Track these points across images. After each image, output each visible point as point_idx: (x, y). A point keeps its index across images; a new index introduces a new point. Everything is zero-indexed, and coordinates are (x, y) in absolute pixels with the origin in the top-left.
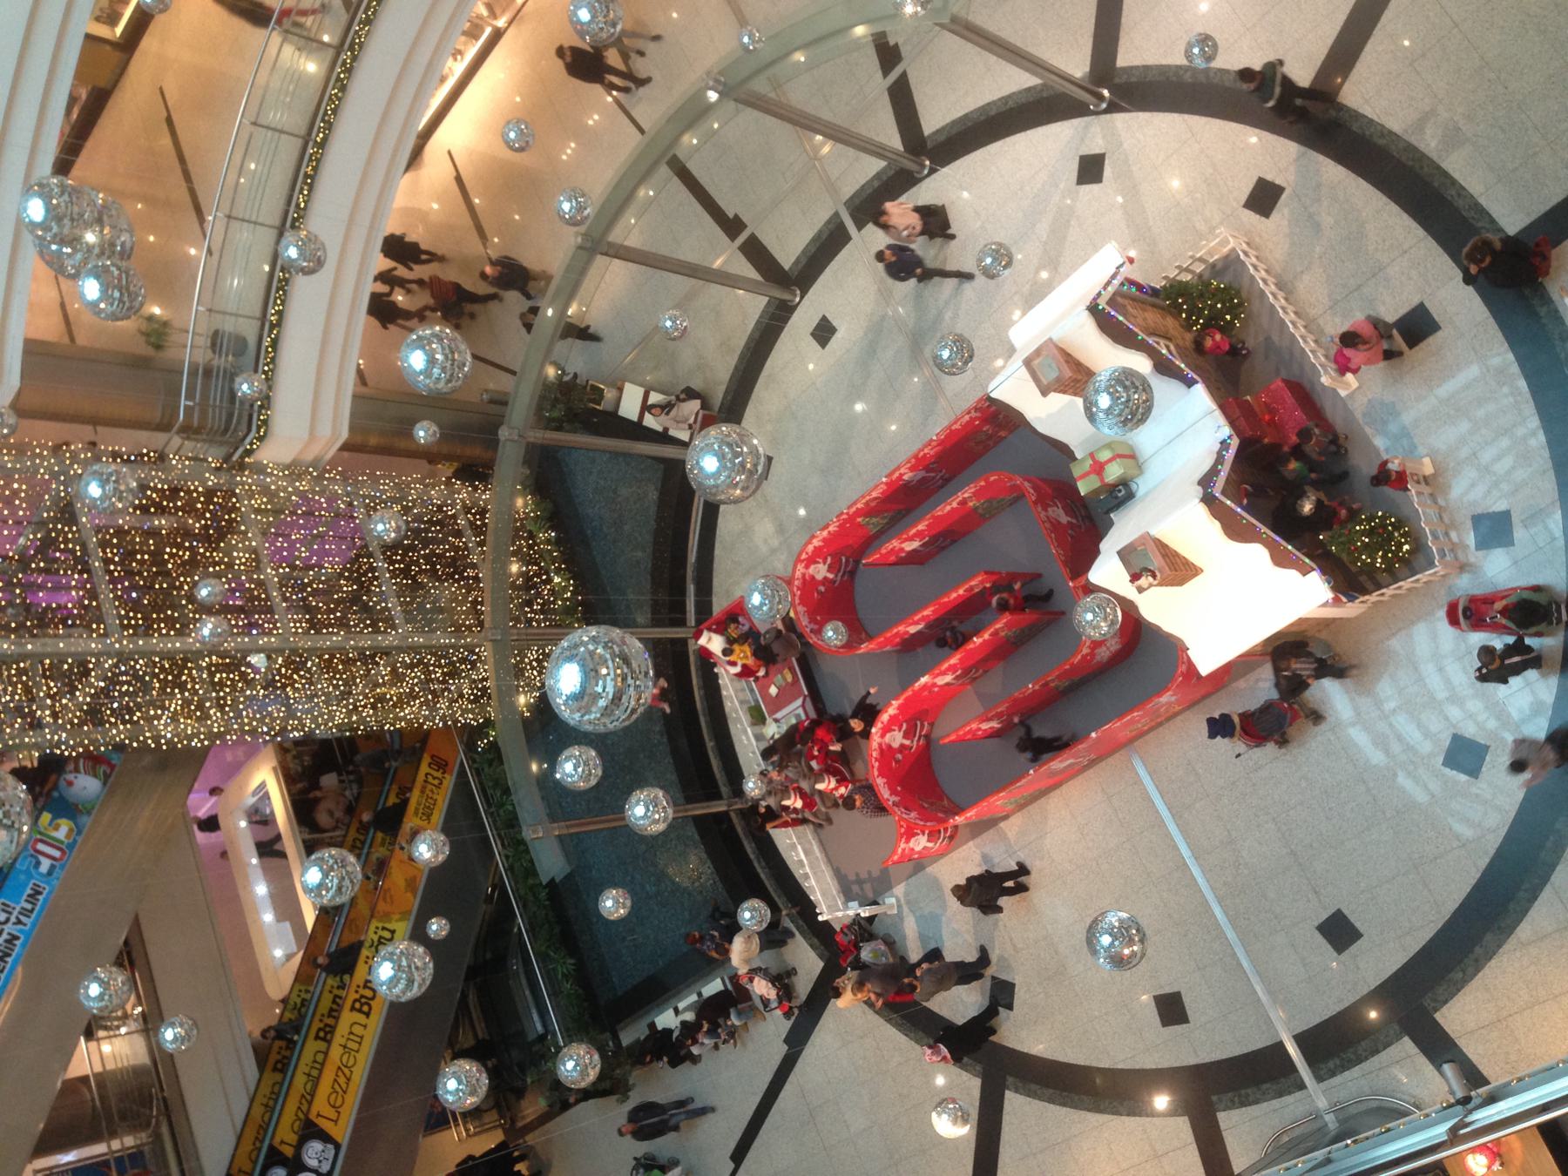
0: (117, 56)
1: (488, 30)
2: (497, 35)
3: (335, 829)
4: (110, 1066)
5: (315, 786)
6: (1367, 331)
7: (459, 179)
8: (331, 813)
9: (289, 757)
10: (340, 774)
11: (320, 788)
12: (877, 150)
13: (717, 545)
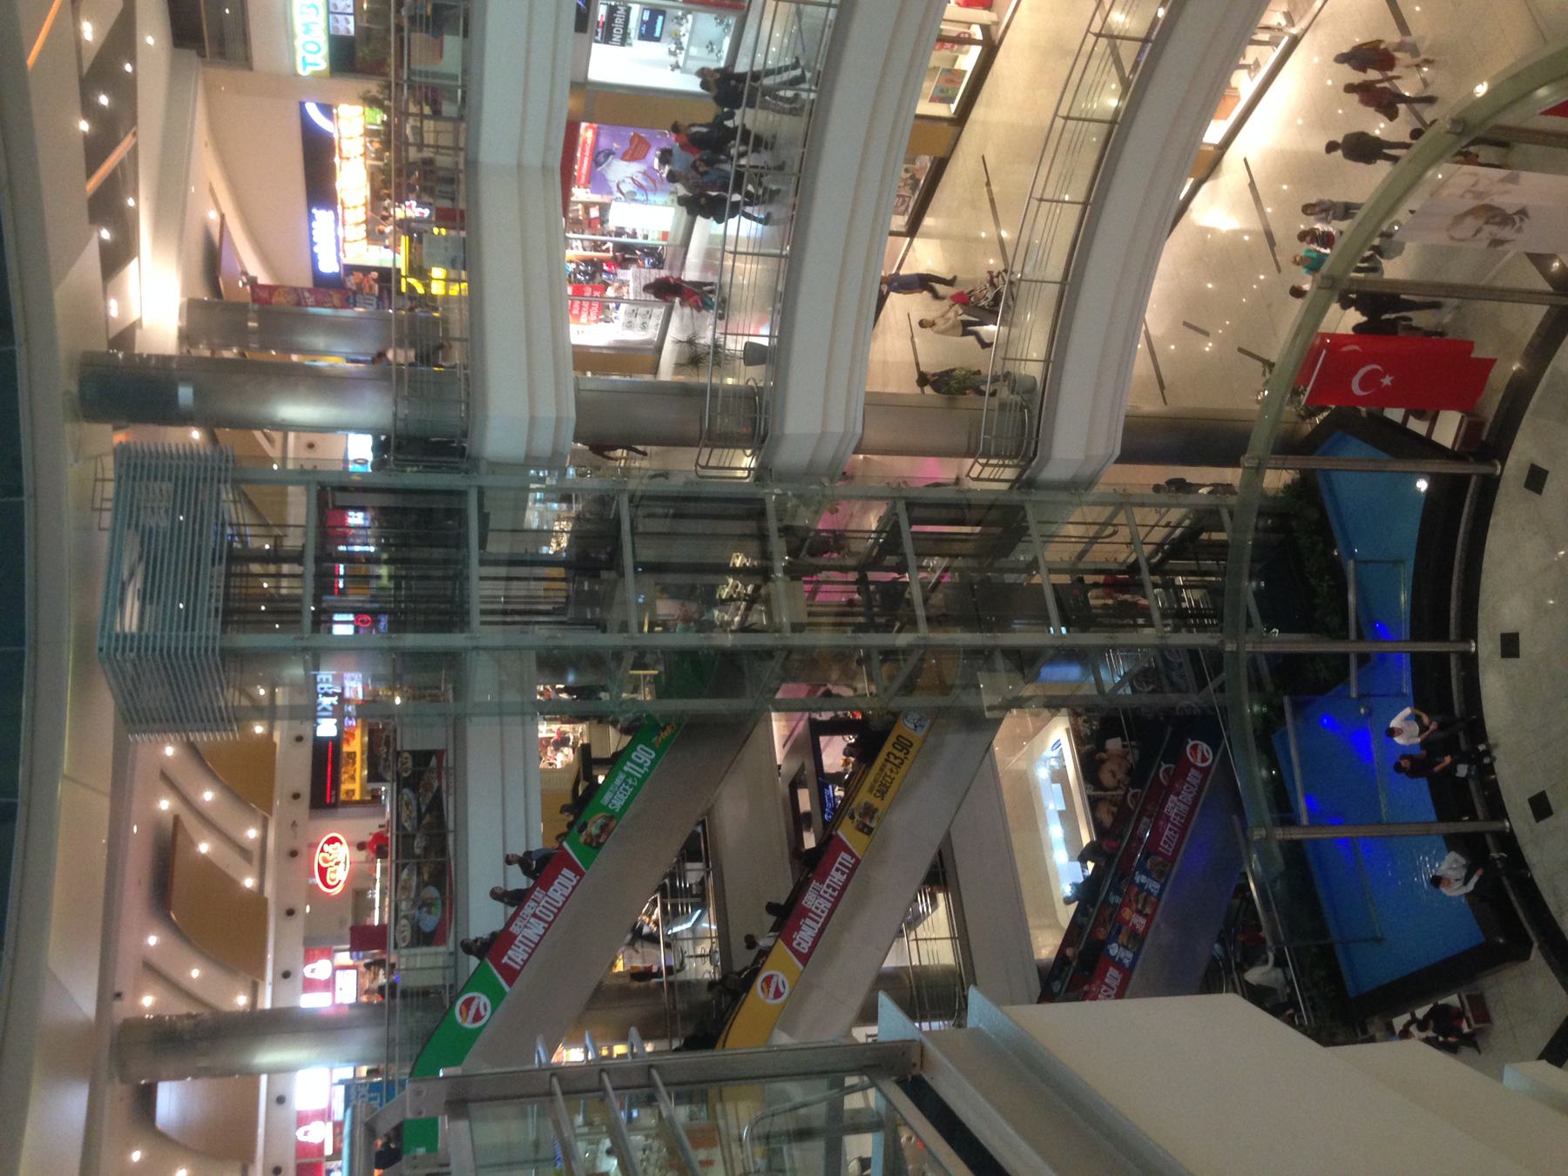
0: (953, 130)
1: (1286, 39)
2: (1295, 42)
3: (1116, 789)
4: (925, 962)
5: (1101, 747)
6: (518, 880)
7: (1252, 185)
8: (1114, 775)
9: (1080, 720)
10: (1123, 739)
11: (1104, 751)
12: (1529, 296)
13: (1486, 558)
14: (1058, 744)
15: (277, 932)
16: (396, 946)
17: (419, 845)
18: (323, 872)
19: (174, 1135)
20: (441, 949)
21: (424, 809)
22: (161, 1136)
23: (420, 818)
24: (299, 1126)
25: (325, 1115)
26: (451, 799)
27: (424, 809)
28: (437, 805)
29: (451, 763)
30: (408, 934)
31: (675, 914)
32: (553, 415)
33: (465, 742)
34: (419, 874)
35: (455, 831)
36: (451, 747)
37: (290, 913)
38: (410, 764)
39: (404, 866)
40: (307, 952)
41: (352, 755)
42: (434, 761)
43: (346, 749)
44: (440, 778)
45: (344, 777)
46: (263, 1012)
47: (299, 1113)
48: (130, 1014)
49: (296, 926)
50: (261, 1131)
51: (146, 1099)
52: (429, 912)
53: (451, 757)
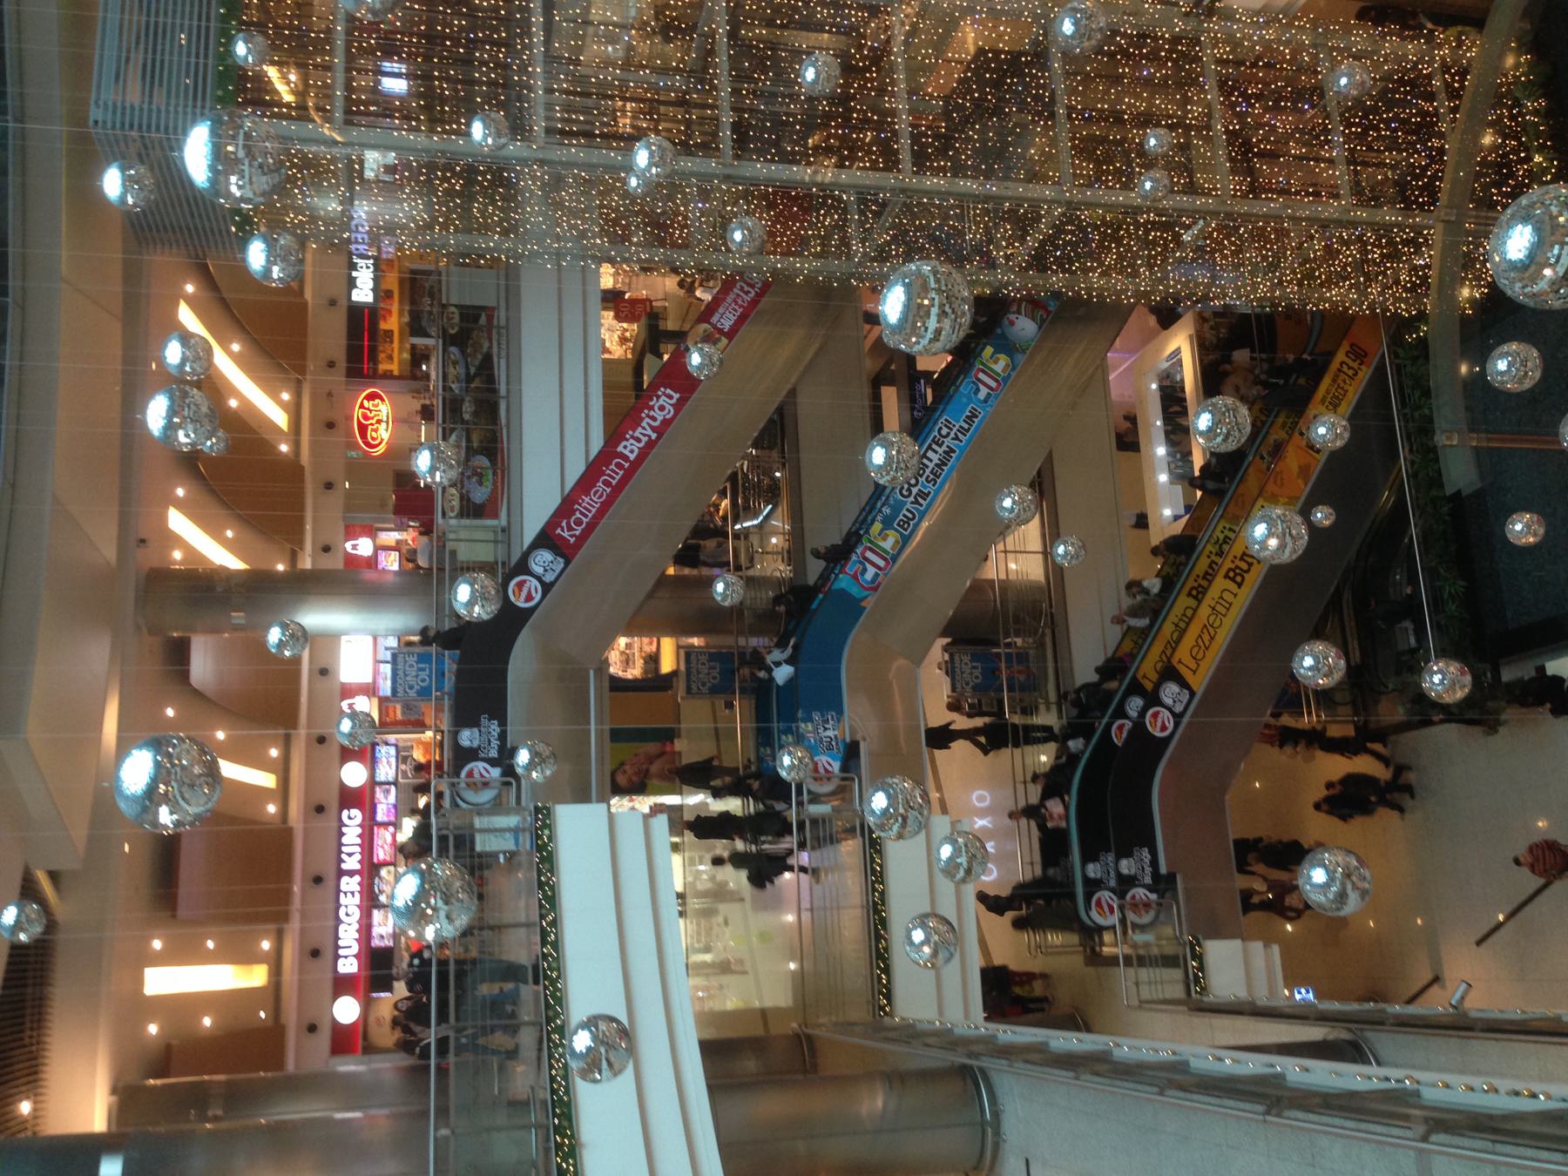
5: (1227, 359)
9: (1206, 327)
10: (1253, 351)
11: (1229, 362)
14: (1178, 351)
15: (315, 510)
16: (444, 514)
17: (468, 409)
18: (363, 429)
19: (207, 693)
20: (490, 522)
21: (473, 370)
22: (197, 693)
23: (469, 379)
24: (343, 699)
25: (370, 690)
26: (503, 362)
27: (473, 370)
28: (486, 368)
29: (503, 323)
30: (456, 503)
31: (747, 508)
32: (505, 921)
33: (518, 295)
34: (469, 440)
35: (507, 397)
36: (503, 304)
37: (329, 486)
38: (457, 319)
39: (452, 430)
40: (347, 527)
41: (389, 333)
42: (483, 320)
43: (383, 326)
44: (490, 340)
45: (382, 356)
46: (304, 571)
47: (343, 685)
48: (155, 564)
49: (336, 500)
50: (304, 699)
51: (178, 653)
52: (481, 484)
53: (503, 313)
